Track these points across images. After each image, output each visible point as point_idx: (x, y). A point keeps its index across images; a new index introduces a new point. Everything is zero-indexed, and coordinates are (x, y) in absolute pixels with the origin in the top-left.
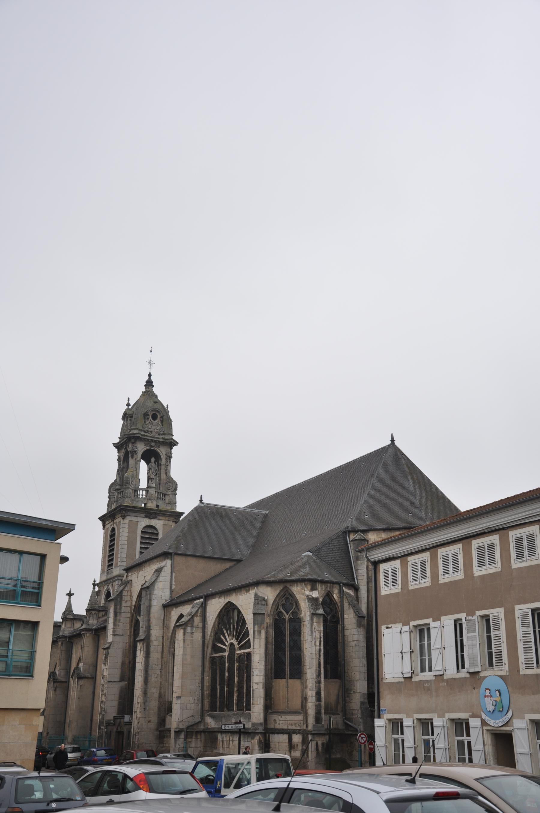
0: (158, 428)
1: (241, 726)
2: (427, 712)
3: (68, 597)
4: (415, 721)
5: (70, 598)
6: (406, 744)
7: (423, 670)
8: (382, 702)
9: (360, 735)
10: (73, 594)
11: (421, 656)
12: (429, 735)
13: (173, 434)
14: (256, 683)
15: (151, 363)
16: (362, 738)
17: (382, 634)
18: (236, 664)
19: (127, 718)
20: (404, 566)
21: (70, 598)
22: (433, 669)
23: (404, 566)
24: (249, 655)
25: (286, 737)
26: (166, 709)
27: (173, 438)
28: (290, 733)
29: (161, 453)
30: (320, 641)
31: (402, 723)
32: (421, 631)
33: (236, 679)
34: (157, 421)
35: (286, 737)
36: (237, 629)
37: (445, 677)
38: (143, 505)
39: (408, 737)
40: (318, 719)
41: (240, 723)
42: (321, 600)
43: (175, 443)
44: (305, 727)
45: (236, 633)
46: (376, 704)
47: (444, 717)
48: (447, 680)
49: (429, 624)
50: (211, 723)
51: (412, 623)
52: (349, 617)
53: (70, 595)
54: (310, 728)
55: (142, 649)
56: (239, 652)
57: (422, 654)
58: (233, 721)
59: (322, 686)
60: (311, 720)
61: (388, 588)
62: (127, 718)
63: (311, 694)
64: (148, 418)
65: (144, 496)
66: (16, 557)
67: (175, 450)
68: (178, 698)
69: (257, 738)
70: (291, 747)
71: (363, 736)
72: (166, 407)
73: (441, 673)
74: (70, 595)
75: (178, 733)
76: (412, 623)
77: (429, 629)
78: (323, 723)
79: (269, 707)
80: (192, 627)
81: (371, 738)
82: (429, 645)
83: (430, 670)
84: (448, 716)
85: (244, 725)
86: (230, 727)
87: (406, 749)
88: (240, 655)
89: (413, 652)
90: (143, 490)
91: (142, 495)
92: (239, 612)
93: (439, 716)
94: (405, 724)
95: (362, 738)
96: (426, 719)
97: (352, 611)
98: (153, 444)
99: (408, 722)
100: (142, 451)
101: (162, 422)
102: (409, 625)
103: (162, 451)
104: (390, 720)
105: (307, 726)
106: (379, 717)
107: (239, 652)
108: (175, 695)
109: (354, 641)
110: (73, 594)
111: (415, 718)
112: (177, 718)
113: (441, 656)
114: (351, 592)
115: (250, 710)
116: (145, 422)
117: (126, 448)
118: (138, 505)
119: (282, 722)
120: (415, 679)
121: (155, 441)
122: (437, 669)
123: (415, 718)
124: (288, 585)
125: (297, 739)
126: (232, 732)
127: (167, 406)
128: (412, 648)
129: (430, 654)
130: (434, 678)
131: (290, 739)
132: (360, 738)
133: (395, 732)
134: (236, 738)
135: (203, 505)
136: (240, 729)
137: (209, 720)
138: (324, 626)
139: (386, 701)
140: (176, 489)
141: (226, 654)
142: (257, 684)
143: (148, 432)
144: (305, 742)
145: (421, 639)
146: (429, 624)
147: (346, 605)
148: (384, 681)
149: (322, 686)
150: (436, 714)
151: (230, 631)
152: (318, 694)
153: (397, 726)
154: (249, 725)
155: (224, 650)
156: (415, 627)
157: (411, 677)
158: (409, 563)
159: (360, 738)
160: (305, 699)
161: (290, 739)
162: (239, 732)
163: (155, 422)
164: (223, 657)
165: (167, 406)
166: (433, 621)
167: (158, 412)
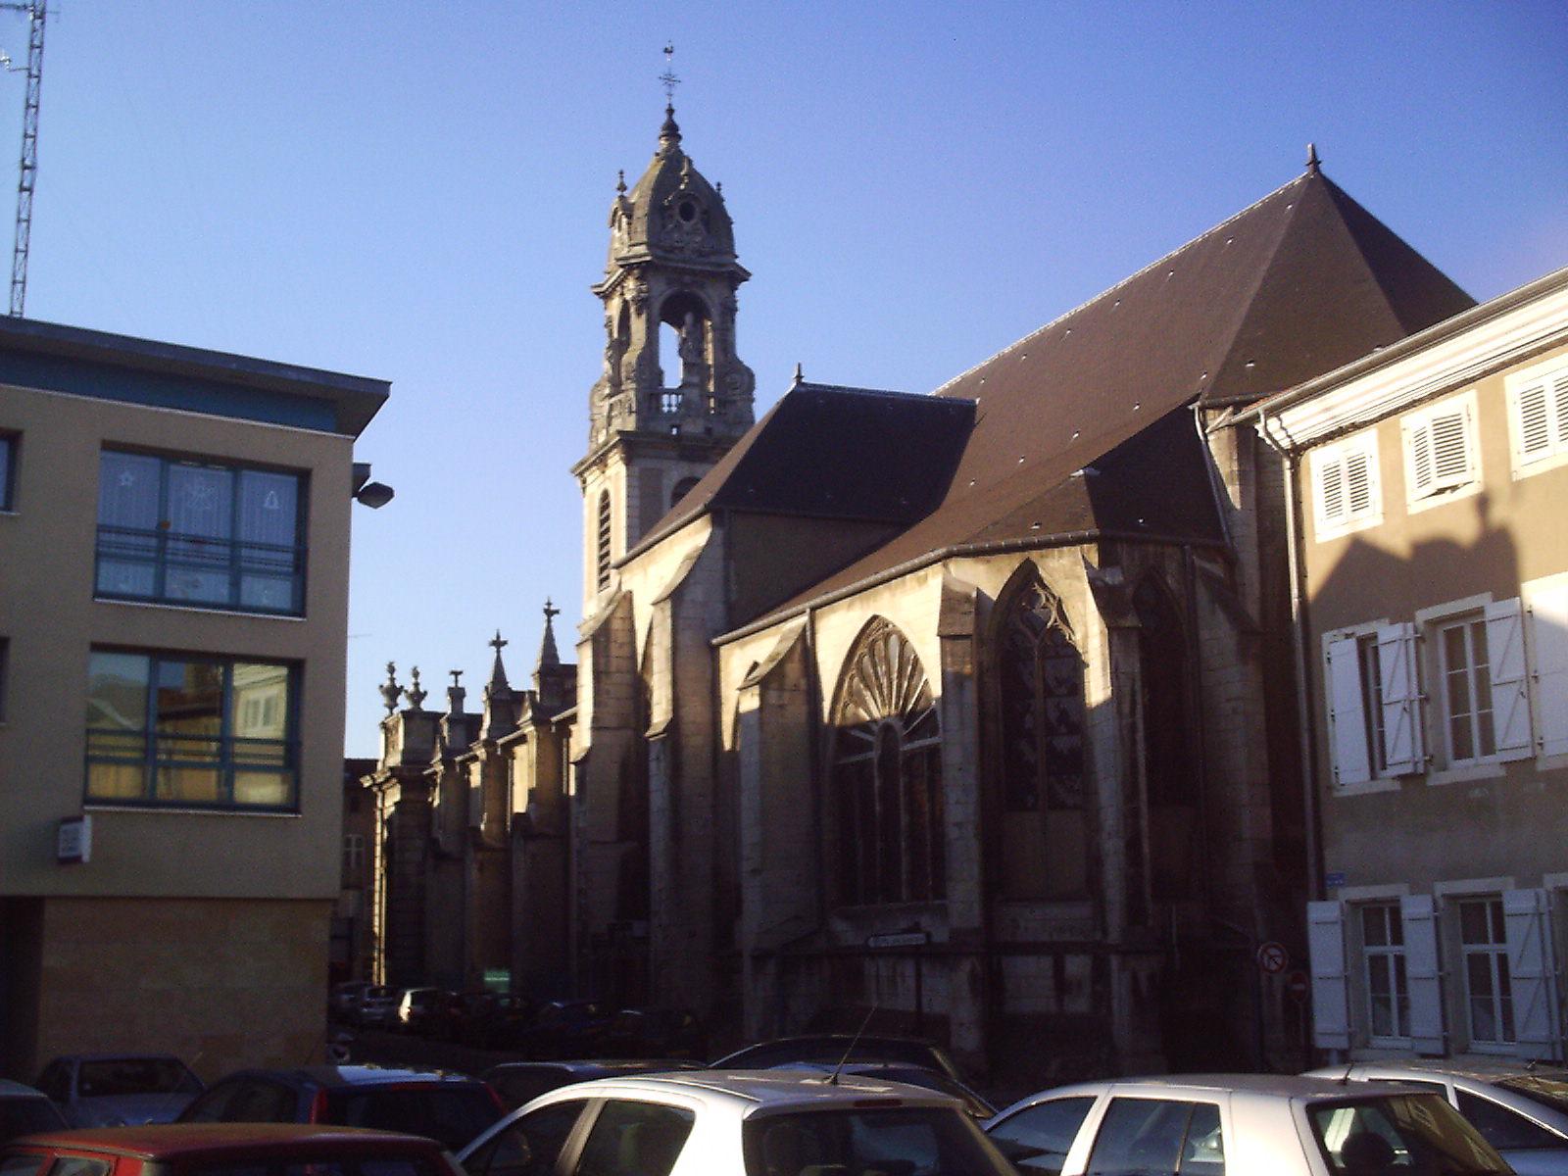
0: (698, 239)
1: (918, 939)
2: (1481, 875)
3: (494, 649)
4: (1441, 903)
5: (498, 652)
6: (1411, 970)
7: (1462, 751)
8: (1330, 856)
9: (1265, 951)
10: (505, 643)
11: (1454, 709)
12: (1485, 941)
13: (737, 253)
14: (956, 824)
15: (669, 80)
16: (1271, 957)
17: (1325, 656)
18: (902, 781)
19: (638, 928)
20: (1391, 447)
21: (498, 652)
22: (1499, 743)
23: (1391, 447)
24: (934, 752)
25: (1046, 963)
26: (727, 902)
27: (737, 261)
28: (1058, 952)
29: (710, 303)
30: (1133, 703)
31: (1498, 908)
32: (1454, 639)
33: (904, 819)
34: (693, 222)
35: (1046, 963)
36: (900, 686)
37: (1541, 767)
38: (675, 431)
39: (1420, 949)
40: (1134, 911)
41: (916, 928)
42: (1129, 591)
43: (743, 276)
44: (1098, 936)
45: (898, 697)
46: (1311, 860)
47: (1541, 885)
48: (1549, 775)
49: (1480, 611)
50: (845, 932)
51: (1422, 615)
52: (1217, 635)
53: (498, 643)
54: (1114, 936)
55: (662, 757)
56: (908, 747)
57: (1458, 702)
58: (903, 924)
59: (1144, 823)
60: (1115, 918)
61: (1337, 520)
62: (638, 928)
63: (1112, 847)
64: (671, 216)
65: (674, 409)
66: (153, 463)
67: (743, 292)
68: (755, 872)
69: (966, 966)
70: (1062, 985)
71: (1273, 952)
72: (715, 188)
73: (1527, 753)
74: (498, 643)
75: (760, 958)
76: (1422, 615)
77: (1480, 630)
78: (1150, 923)
79: (997, 885)
80: (781, 689)
81: (1299, 961)
82: (1483, 677)
83: (1488, 747)
84: (1442, 888)
85: (929, 935)
86: (891, 941)
87: (1411, 986)
88: (912, 755)
89: (1427, 699)
90: (670, 392)
91: (670, 405)
92: (903, 642)
93: (1522, 884)
94: (1406, 912)
95: (1272, 958)
96: (1474, 896)
97: (1221, 616)
98: (687, 279)
99: (1416, 908)
100: (662, 299)
101: (707, 223)
102: (1412, 619)
103: (712, 295)
104: (1355, 905)
105: (1105, 932)
106: (1322, 897)
107: (908, 747)
108: (746, 867)
109: (1228, 700)
110: (505, 643)
111: (1438, 894)
112: (753, 923)
113: (1523, 702)
114: (1217, 569)
115: (944, 896)
116: (664, 226)
117: (622, 294)
118: (662, 428)
119: (1033, 921)
120: (1437, 779)
121: (693, 273)
122: (1509, 743)
123: (1438, 894)
124: (1034, 555)
125: (1077, 966)
126: (900, 953)
127: (719, 185)
128: (1426, 688)
129: (1485, 700)
130: (1502, 772)
131: (1059, 969)
132: (1266, 958)
133: (1373, 936)
134: (908, 968)
135: (803, 389)
136: (918, 947)
137: (840, 926)
138: (1142, 661)
139: (1345, 849)
140: (751, 387)
141: (874, 755)
142: (959, 825)
143: (672, 250)
144: (1100, 972)
145: (1455, 658)
146: (1480, 611)
147: (1202, 595)
148: (1336, 794)
149: (1144, 823)
150: (1511, 880)
151: (881, 693)
152: (1133, 845)
153: (1378, 921)
154: (941, 935)
155: (868, 746)
156: (1434, 624)
157: (1424, 776)
158: (1404, 433)
159: (1266, 958)
160: (1095, 860)
161: (1059, 969)
162: (918, 954)
163: (687, 225)
164: (868, 763)
165: (719, 185)
166: (1496, 598)
167: (695, 198)
